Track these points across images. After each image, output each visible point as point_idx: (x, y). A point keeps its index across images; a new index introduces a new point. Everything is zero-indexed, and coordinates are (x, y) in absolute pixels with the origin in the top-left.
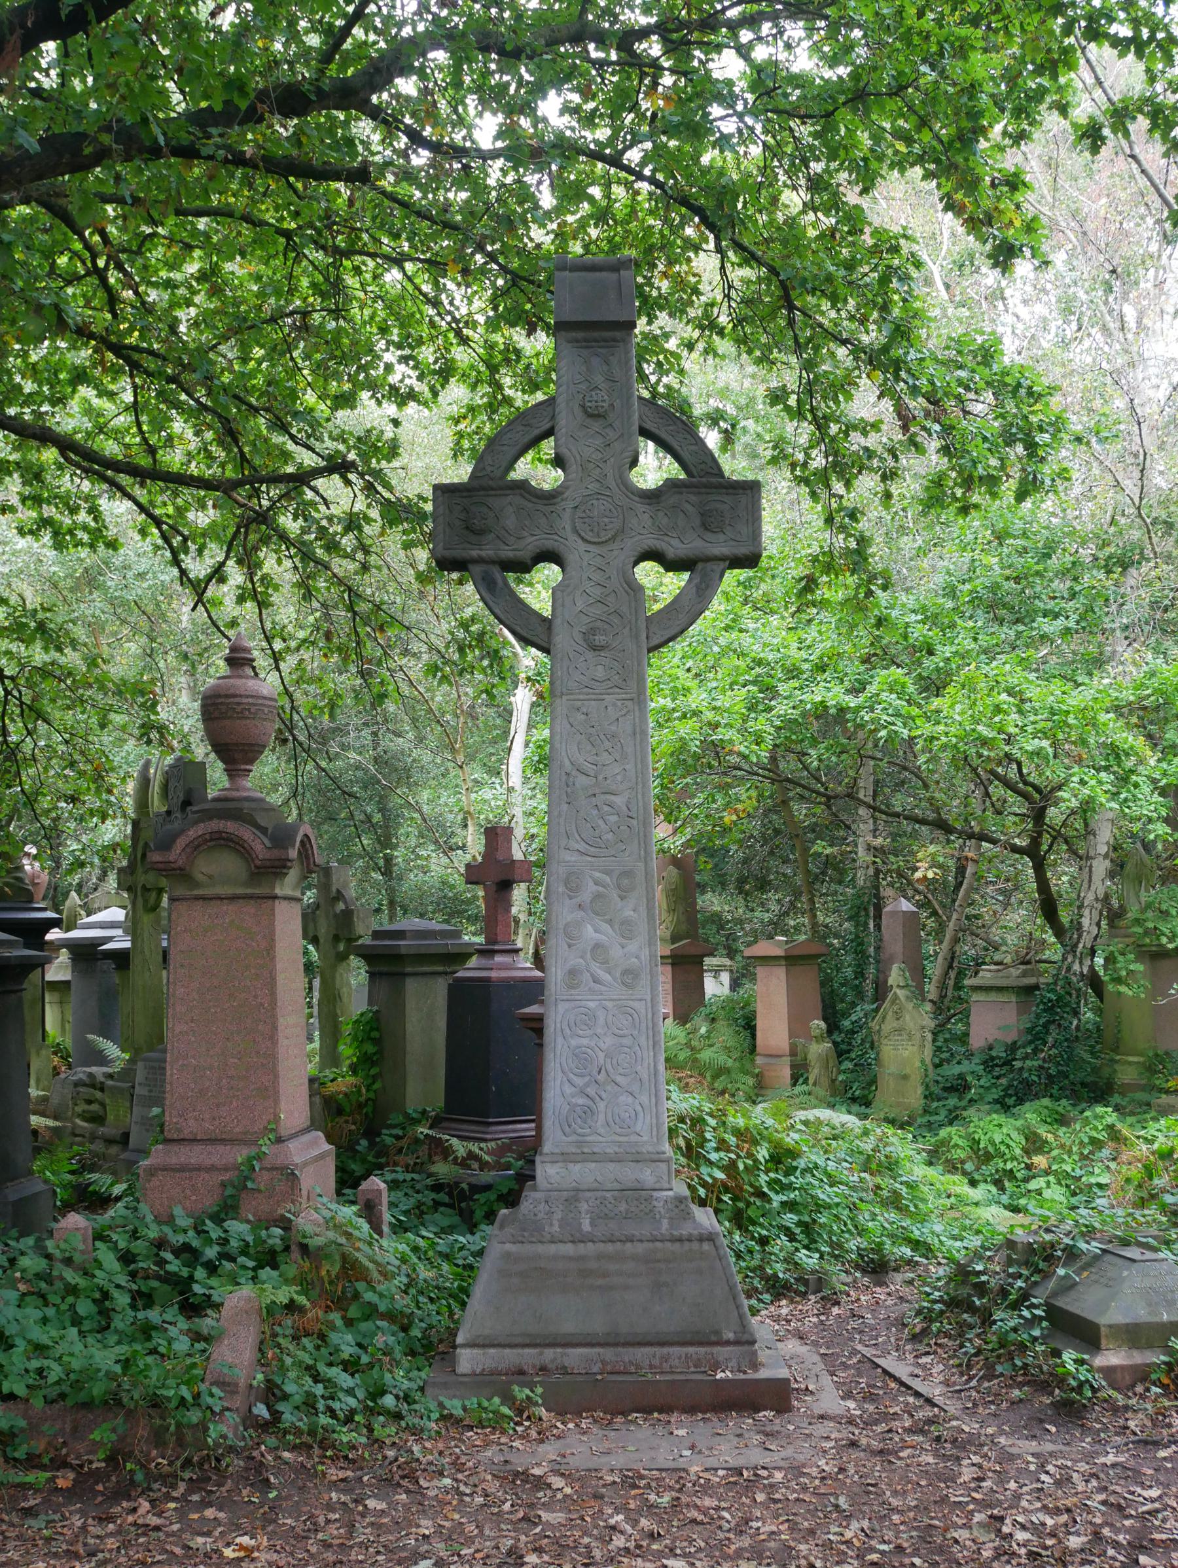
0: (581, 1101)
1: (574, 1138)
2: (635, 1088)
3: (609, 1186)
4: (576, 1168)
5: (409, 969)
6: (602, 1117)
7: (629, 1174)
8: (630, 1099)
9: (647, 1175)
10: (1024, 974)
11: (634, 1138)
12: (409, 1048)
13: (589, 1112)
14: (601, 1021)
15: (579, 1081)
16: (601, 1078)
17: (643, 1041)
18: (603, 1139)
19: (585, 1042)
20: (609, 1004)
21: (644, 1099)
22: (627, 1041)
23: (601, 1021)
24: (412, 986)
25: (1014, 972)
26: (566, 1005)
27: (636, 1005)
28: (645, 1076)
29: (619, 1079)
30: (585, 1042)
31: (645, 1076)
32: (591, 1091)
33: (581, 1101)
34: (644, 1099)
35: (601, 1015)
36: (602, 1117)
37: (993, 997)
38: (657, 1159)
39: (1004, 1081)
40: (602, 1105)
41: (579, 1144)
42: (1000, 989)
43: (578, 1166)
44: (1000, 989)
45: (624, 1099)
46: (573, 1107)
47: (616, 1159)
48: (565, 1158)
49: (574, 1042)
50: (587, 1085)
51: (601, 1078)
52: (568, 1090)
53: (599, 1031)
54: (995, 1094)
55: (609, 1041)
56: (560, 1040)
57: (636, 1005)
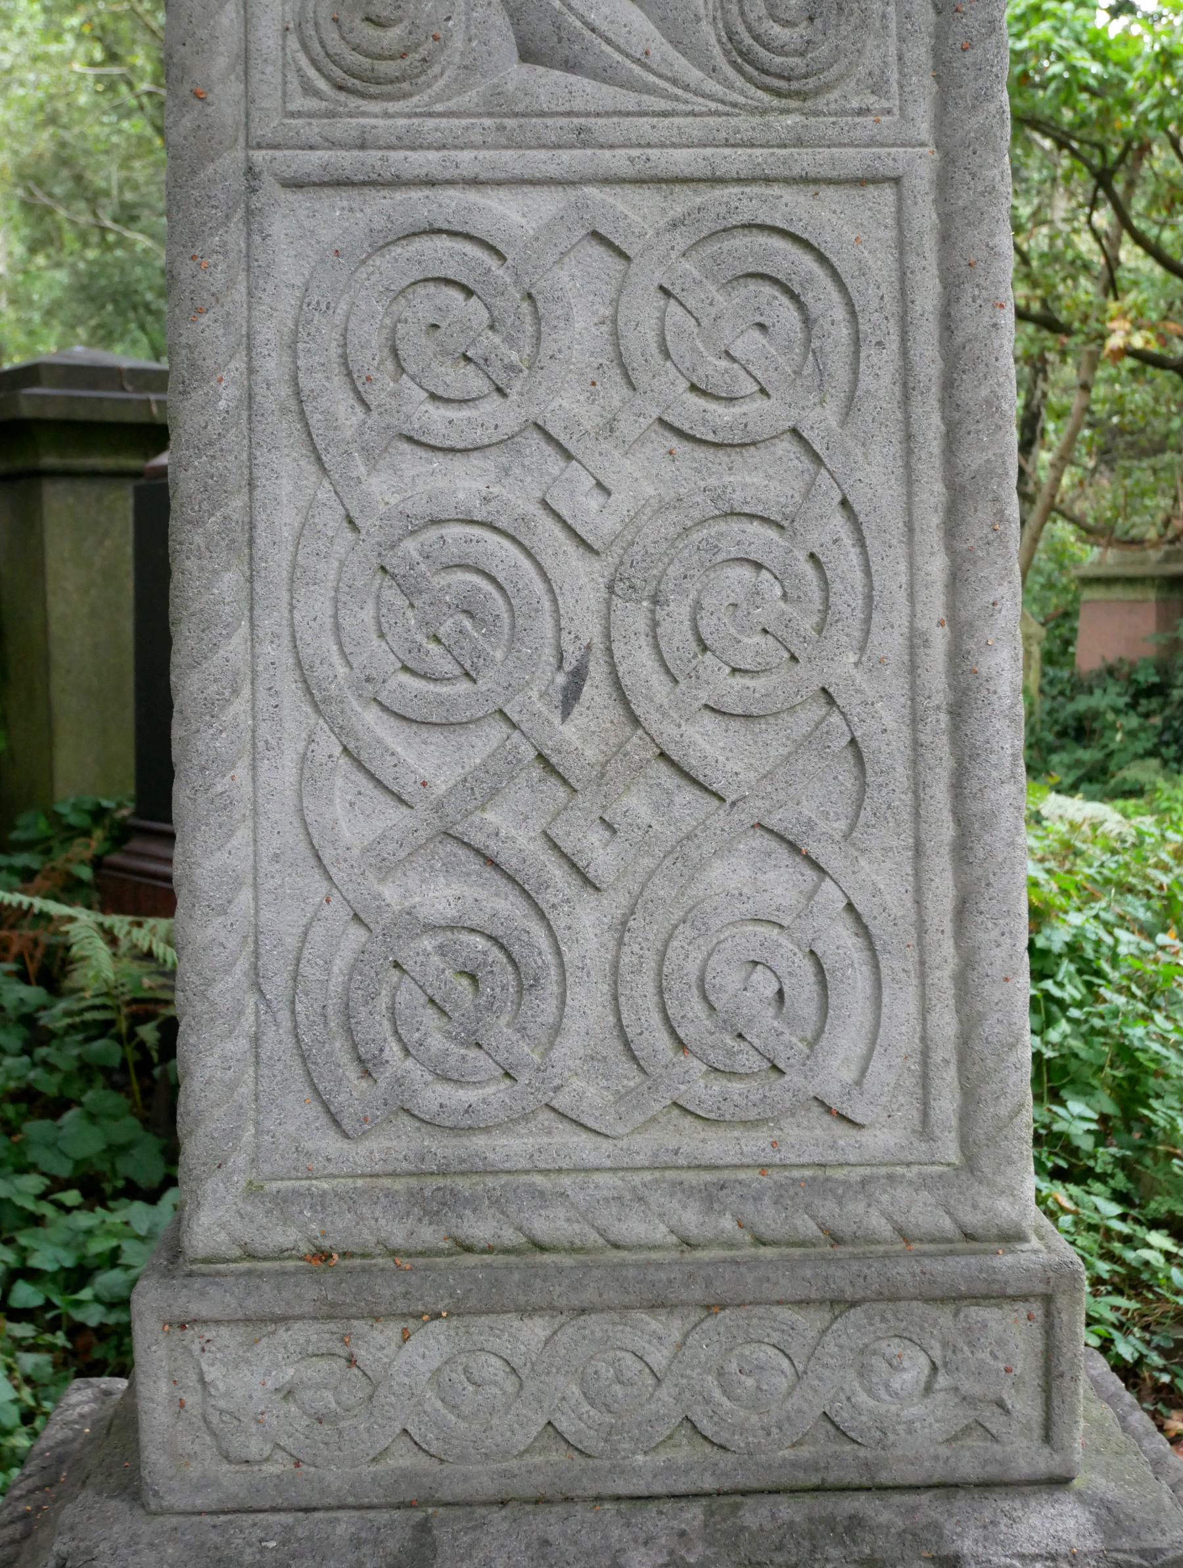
0: (440, 894)
1: (395, 1144)
2: (819, 803)
3: (644, 1468)
4: (414, 1358)
5: (50, 461)
6: (588, 1003)
7: (779, 1384)
8: (783, 882)
9: (899, 1394)
10: (1168, 558)
11: (806, 1139)
12: (58, 656)
13: (501, 973)
14: (580, 331)
15: (430, 763)
16: (583, 735)
17: (875, 476)
18: (587, 1151)
19: (466, 482)
20: (636, 213)
21: (880, 879)
22: (768, 479)
23: (580, 331)
24: (59, 504)
25: (1154, 555)
26: (339, 218)
27: (831, 217)
28: (885, 725)
29: (706, 743)
30: (466, 482)
31: (885, 725)
32: (511, 826)
33: (440, 894)
34: (880, 879)
35: (579, 288)
36: (588, 1003)
37: (1118, 593)
38: (953, 1280)
39: (1157, 721)
40: (587, 924)
41: (435, 1191)
42: (1130, 581)
43: (432, 1346)
44: (1130, 581)
45: (744, 875)
46: (389, 939)
47: (698, 1289)
48: (337, 1282)
49: (387, 487)
50: (485, 787)
51: (583, 735)
52: (355, 820)
53: (567, 406)
54: (1146, 742)
55: (638, 480)
56: (287, 482)
57: (831, 217)
